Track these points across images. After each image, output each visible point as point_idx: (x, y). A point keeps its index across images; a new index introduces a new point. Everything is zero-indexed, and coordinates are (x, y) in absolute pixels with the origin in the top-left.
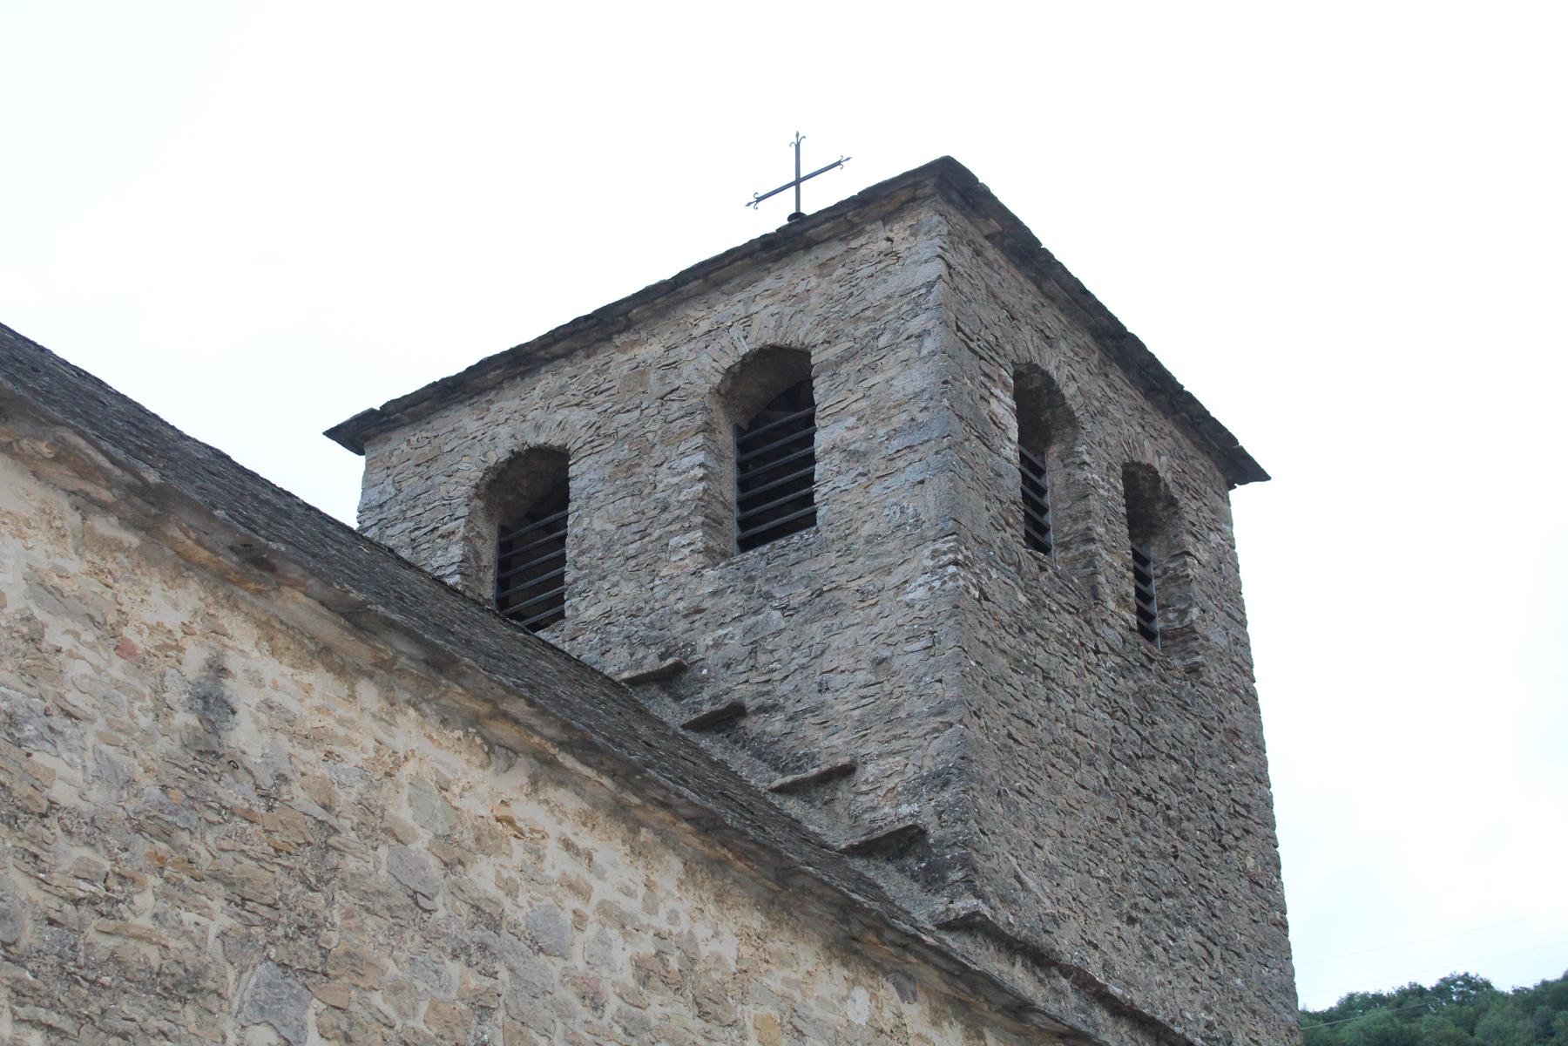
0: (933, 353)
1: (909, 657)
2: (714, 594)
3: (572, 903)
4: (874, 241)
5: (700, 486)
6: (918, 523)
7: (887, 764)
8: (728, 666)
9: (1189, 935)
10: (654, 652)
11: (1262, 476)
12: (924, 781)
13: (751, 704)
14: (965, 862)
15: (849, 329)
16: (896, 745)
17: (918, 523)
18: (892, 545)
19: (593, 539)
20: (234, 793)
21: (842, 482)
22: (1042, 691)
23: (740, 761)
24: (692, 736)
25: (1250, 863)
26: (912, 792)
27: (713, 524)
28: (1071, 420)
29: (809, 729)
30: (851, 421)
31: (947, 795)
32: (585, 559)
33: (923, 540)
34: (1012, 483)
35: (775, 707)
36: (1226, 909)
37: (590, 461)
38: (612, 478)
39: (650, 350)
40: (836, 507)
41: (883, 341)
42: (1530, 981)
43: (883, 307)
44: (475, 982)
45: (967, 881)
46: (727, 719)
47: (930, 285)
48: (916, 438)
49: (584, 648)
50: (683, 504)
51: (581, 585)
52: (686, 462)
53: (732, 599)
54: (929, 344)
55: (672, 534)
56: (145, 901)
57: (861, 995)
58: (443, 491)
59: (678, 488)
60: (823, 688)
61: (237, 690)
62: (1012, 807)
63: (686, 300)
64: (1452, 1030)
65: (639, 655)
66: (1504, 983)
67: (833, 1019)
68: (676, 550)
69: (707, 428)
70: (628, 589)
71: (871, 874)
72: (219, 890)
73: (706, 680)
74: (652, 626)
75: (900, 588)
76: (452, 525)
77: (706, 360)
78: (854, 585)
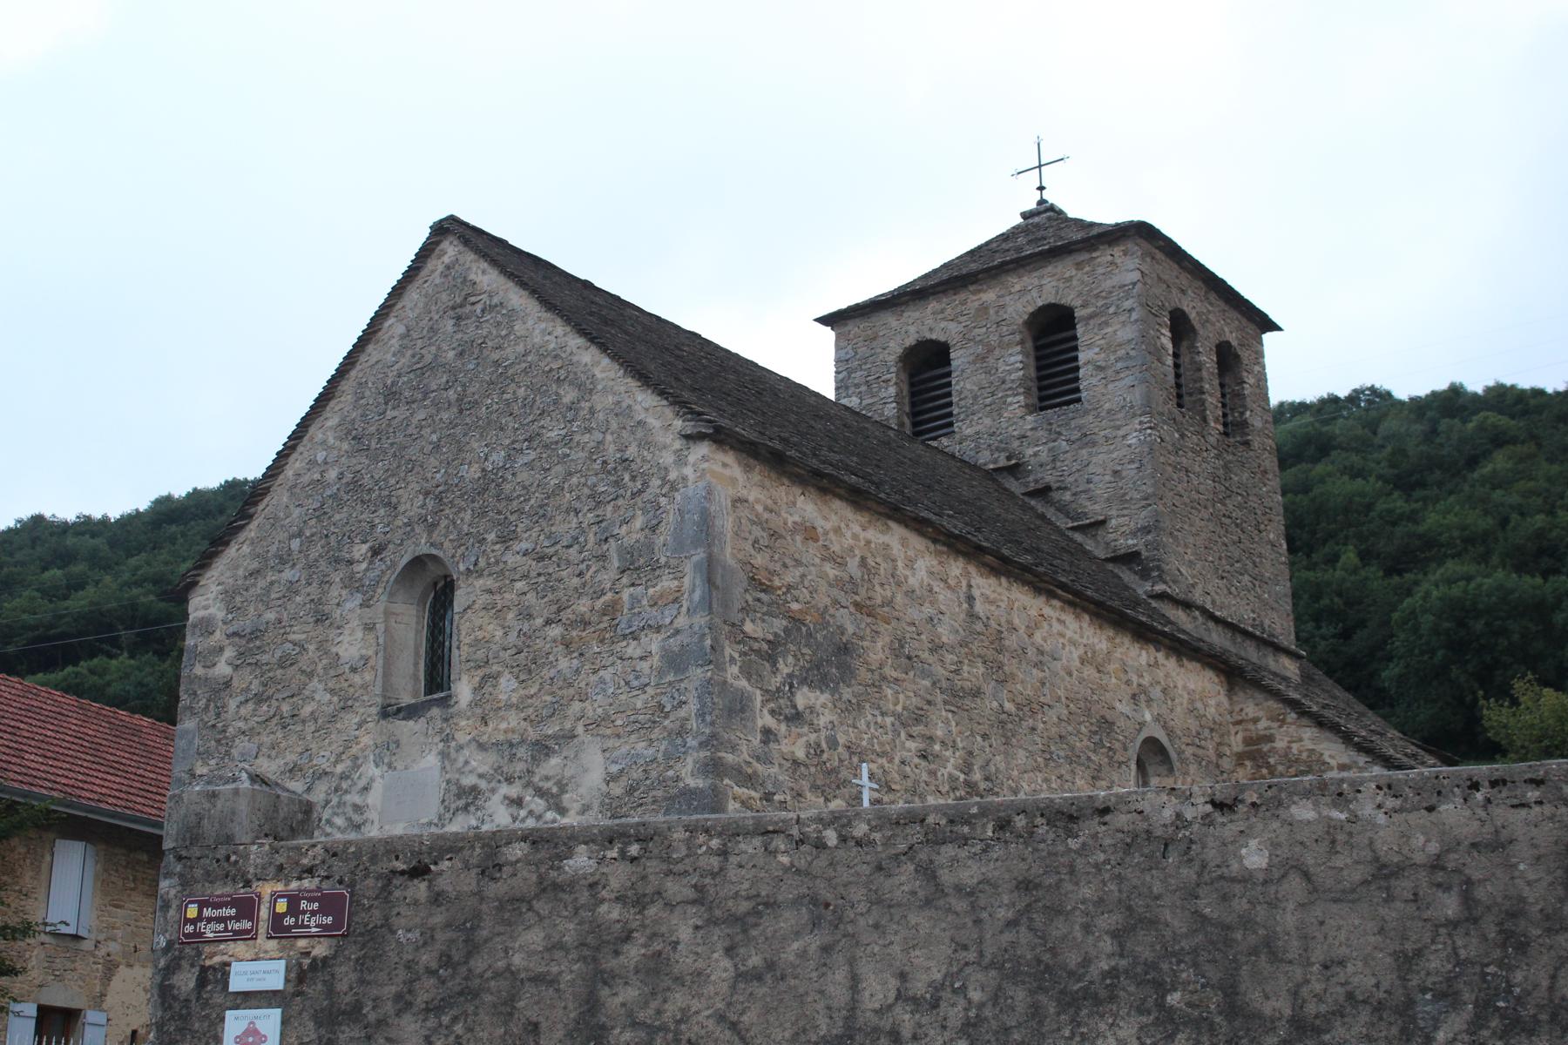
0: (1136, 321)
1: (1130, 471)
2: (1032, 429)
3: (1061, 640)
4: (1104, 256)
5: (1021, 373)
6: (1132, 407)
7: (1121, 520)
8: (1041, 466)
9: (1246, 578)
10: (1003, 455)
11: (1279, 329)
12: (1139, 530)
13: (1055, 486)
14: (1158, 568)
15: (1093, 301)
16: (1125, 512)
17: (1132, 407)
18: (1120, 416)
19: (966, 393)
20: (979, 627)
21: (1094, 381)
22: (1186, 479)
23: (1050, 513)
24: (1027, 499)
25: (1271, 536)
26: (1134, 534)
27: (1027, 392)
28: (1193, 330)
29: (1083, 499)
30: (1097, 350)
31: (1149, 537)
32: (962, 403)
33: (1134, 415)
34: (1171, 379)
35: (1066, 488)
36: (1261, 562)
37: (961, 352)
38: (974, 362)
39: (989, 296)
40: (1091, 393)
41: (1112, 310)
42: (1422, 390)
43: (1111, 292)
44: (1041, 675)
45: (1160, 576)
46: (1043, 492)
47: (1134, 284)
48: (1130, 363)
49: (965, 450)
50: (1013, 381)
51: (962, 416)
52: (1013, 359)
53: (1041, 433)
54: (1134, 316)
55: (1007, 396)
56: (965, 668)
57: (1144, 653)
58: (881, 357)
59: (1010, 372)
60: (1089, 482)
61: (976, 593)
62: (1176, 538)
63: (1008, 271)
64: (1359, 432)
65: (996, 456)
66: (1402, 393)
67: (1136, 664)
68: (1010, 404)
69: (1022, 342)
70: (987, 421)
71: (1116, 571)
72: (980, 660)
73: (1031, 471)
74: (1001, 441)
75: (1124, 437)
76: (889, 376)
77: (1019, 306)
78: (1102, 433)
